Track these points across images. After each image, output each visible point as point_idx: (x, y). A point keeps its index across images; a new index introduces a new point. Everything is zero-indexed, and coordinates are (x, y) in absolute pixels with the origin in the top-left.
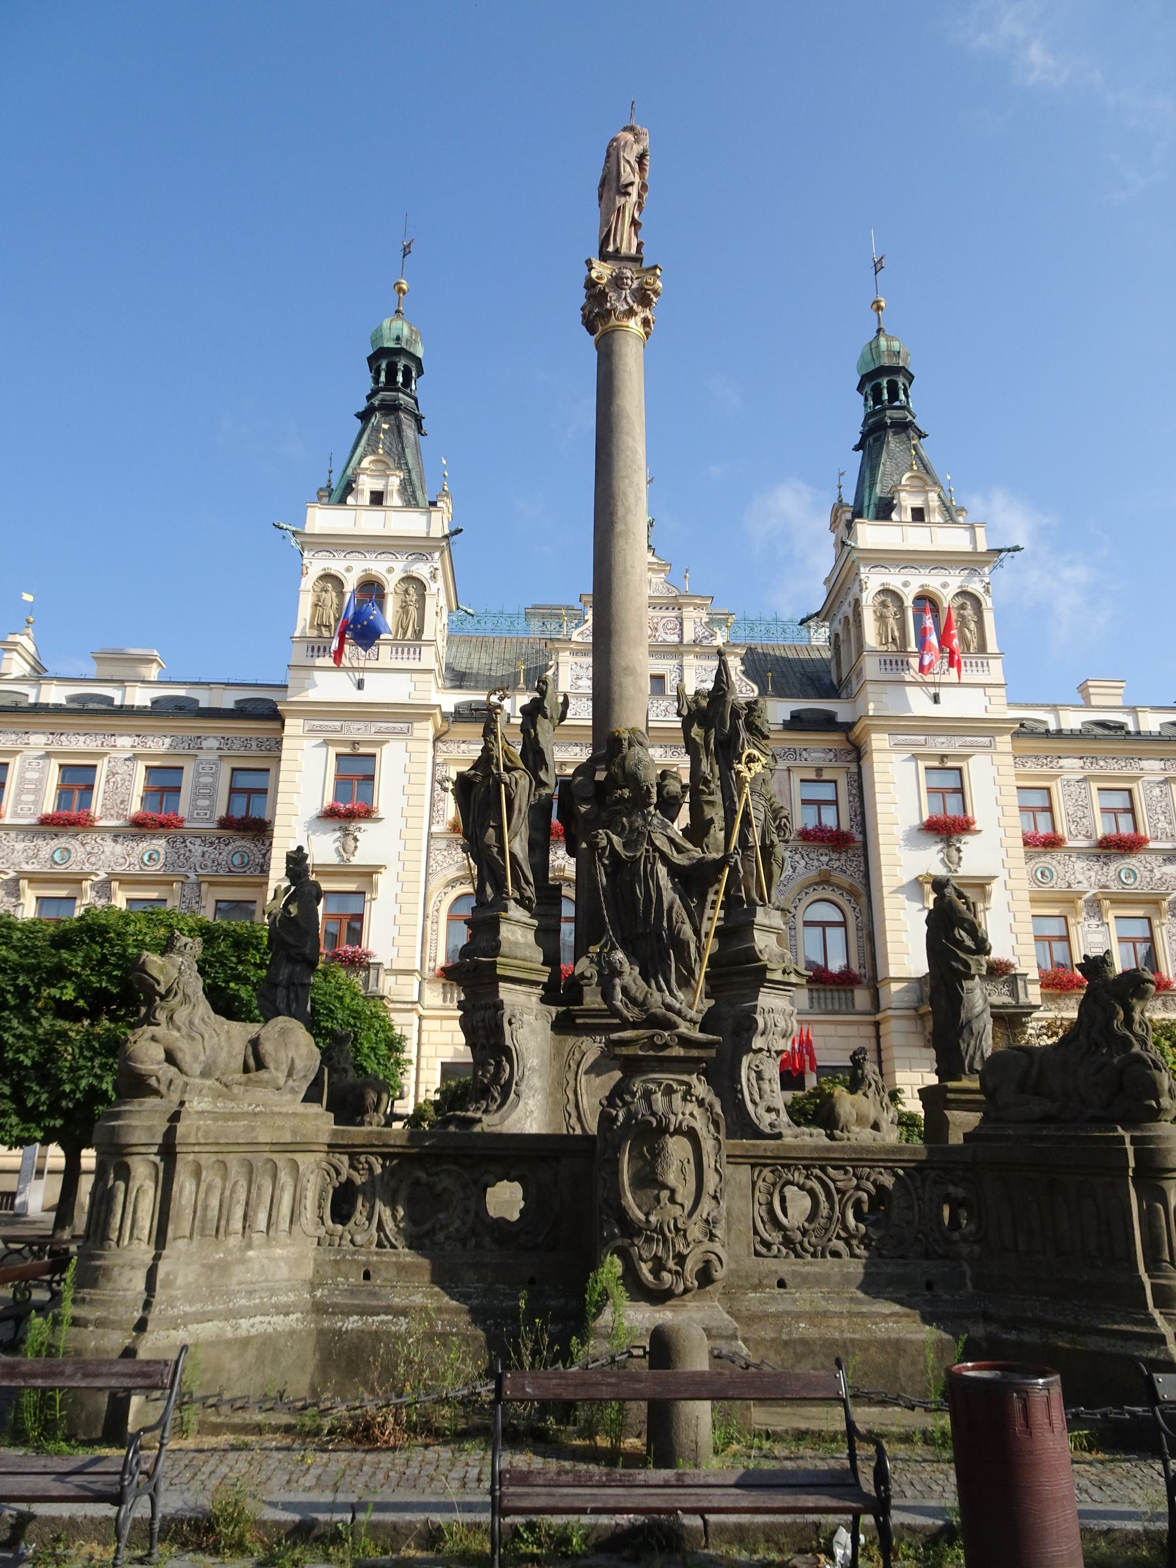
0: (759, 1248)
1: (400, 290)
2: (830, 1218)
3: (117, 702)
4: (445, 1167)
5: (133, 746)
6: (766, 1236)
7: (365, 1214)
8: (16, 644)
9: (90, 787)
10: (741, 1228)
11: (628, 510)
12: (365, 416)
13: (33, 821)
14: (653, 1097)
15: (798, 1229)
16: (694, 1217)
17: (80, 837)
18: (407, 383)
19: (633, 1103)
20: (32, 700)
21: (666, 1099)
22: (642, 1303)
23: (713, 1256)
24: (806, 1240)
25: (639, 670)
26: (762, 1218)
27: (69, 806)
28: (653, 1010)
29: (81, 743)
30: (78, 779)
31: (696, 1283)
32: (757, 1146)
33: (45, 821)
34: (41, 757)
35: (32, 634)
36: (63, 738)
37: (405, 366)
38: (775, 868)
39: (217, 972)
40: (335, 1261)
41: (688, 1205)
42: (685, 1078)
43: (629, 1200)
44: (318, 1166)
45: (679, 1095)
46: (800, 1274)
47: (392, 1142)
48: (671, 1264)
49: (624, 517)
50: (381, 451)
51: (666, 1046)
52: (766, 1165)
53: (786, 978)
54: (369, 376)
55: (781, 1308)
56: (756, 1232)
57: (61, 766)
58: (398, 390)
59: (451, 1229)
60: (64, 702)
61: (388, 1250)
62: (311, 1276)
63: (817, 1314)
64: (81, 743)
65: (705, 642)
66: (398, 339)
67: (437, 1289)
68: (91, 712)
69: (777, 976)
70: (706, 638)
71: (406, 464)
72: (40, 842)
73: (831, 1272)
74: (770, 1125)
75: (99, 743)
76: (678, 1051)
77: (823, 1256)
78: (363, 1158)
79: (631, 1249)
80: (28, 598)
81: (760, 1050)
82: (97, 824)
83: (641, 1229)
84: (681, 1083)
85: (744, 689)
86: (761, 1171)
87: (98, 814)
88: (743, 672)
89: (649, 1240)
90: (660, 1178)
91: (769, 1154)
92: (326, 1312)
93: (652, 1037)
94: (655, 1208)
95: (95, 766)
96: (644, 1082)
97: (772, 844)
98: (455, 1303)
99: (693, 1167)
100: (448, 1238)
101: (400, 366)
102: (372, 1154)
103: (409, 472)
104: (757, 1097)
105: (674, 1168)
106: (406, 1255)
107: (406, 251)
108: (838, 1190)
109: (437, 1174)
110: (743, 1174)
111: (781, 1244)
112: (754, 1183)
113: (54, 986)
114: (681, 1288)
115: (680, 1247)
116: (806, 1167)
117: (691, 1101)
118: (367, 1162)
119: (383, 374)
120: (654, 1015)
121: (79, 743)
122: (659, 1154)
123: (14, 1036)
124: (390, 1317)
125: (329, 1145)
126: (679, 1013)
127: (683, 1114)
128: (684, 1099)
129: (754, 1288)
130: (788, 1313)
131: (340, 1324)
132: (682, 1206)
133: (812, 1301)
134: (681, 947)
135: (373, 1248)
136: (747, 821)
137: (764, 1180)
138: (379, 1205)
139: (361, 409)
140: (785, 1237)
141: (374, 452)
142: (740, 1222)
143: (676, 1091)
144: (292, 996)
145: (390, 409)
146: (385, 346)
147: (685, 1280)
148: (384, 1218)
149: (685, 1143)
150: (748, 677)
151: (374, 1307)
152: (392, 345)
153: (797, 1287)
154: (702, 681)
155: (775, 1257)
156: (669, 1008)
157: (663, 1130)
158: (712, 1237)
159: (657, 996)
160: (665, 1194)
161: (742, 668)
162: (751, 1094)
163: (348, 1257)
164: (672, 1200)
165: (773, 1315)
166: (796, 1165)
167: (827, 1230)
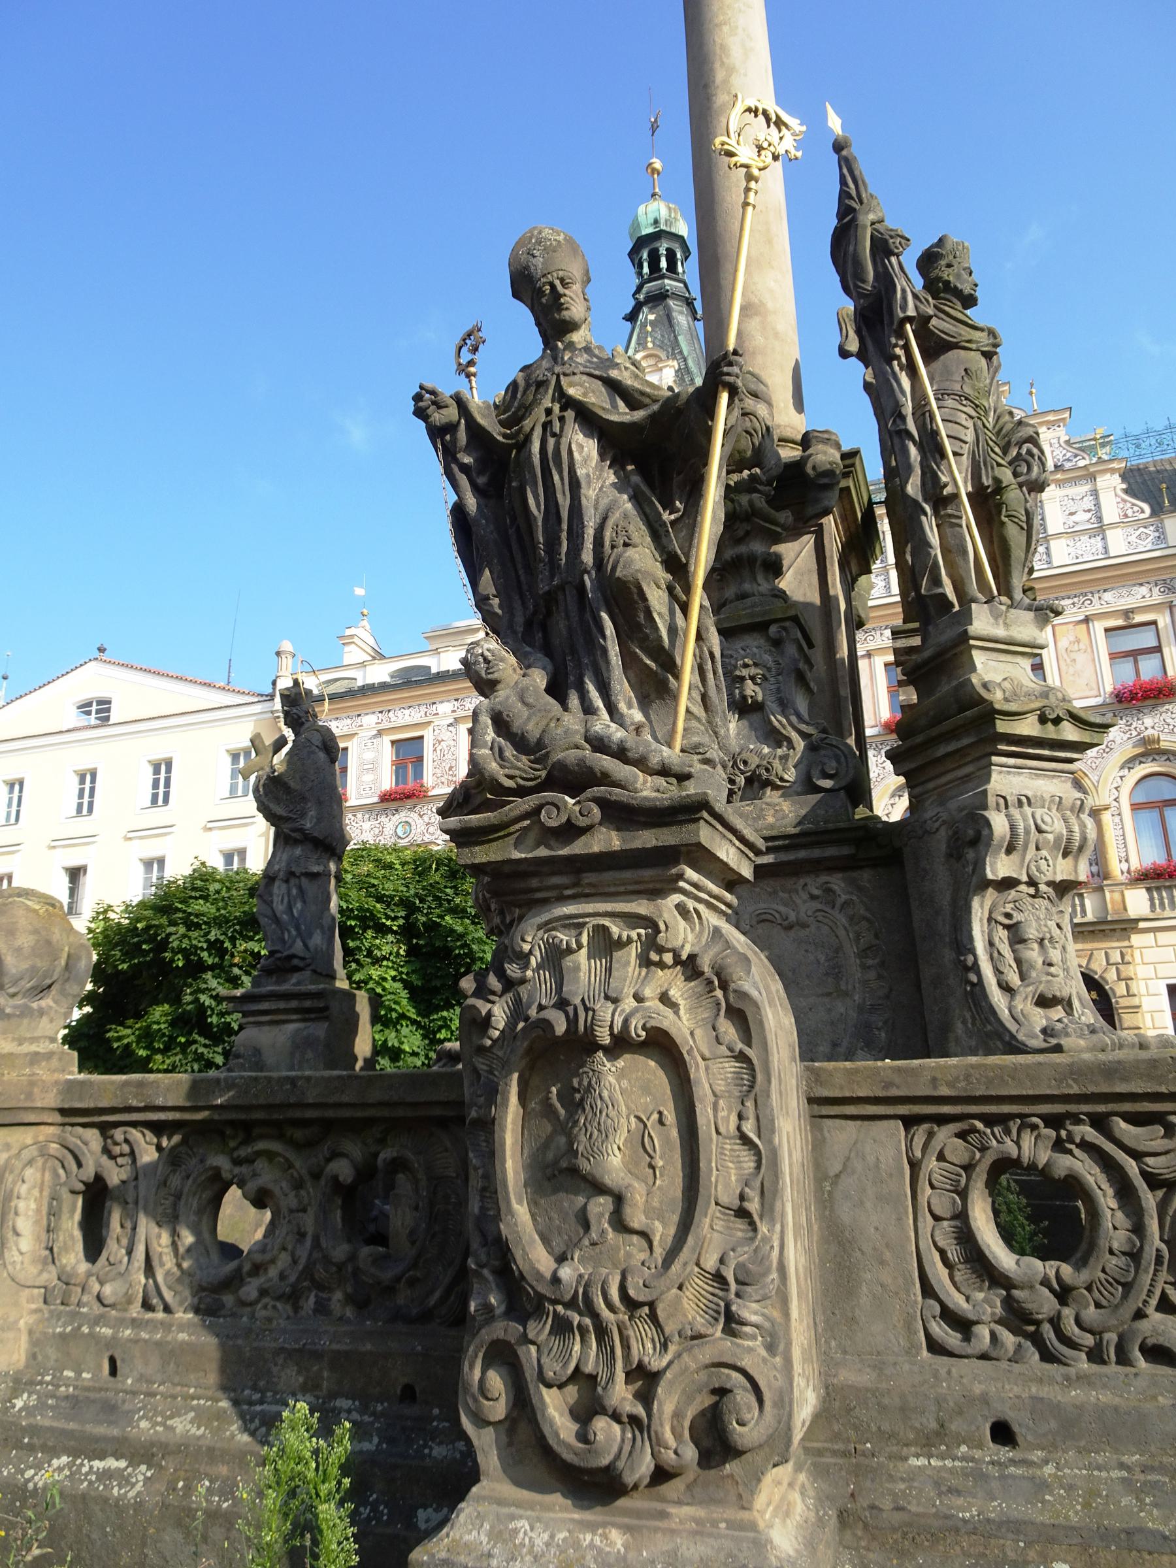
0: (939, 1330)
1: (654, 170)
2: (1135, 1256)
3: (434, 670)
4: (261, 1145)
5: (454, 711)
6: (957, 1301)
7: (125, 1242)
8: (352, 636)
9: (420, 759)
10: (886, 1276)
11: (731, 70)
12: (632, 317)
13: (376, 800)
14: (568, 962)
15: (1045, 1282)
16: (675, 1268)
17: (417, 809)
18: (672, 267)
19: (523, 981)
20: (360, 683)
21: (599, 965)
22: (557, 1498)
23: (735, 1375)
24: (1068, 1313)
25: (770, 305)
26: (942, 1252)
27: (405, 782)
28: (557, 756)
29: (407, 717)
30: (409, 753)
31: (690, 1453)
32: (912, 1072)
33: (386, 798)
34: (375, 737)
35: (368, 627)
36: (391, 714)
37: (667, 250)
38: (1014, 534)
39: (430, 908)
40: (63, 1336)
41: (663, 1233)
42: (641, 907)
43: (519, 1214)
44: (43, 1153)
45: (633, 951)
46: (1056, 1409)
47: (160, 1102)
48: (621, 1394)
49: (726, 81)
50: (650, 345)
51: (571, 831)
52: (942, 1120)
53: (1050, 732)
54: (631, 270)
55: (995, 1508)
56: (928, 1290)
57: (393, 742)
58: (663, 277)
59: (273, 1272)
60: (388, 680)
61: (160, 1315)
62: (22, 1364)
63: (1106, 1535)
64: (407, 717)
65: (1067, 465)
66: (656, 222)
67: (224, 1404)
68: (414, 681)
69: (1028, 727)
70: (1069, 460)
71: (681, 352)
72: (383, 819)
73: (1148, 1406)
74: (1044, 1031)
75: (423, 713)
76: (606, 840)
77: (1123, 1359)
78: (118, 1134)
79: (521, 1351)
80: (359, 592)
81: (1008, 884)
82: (430, 794)
83: (541, 1298)
84: (633, 920)
85: (1130, 513)
86: (931, 1135)
87: (430, 784)
88: (1126, 491)
89: (562, 1328)
90: (584, 1166)
91: (944, 1091)
92: (19, 1446)
93: (537, 810)
94: (578, 1244)
95: (422, 737)
96: (547, 926)
97: (999, 488)
98: (245, 1438)
99: (674, 1133)
100: (263, 1292)
101: (663, 251)
102: (134, 1124)
103: (685, 360)
104: (1014, 979)
105: (621, 1138)
106: (182, 1328)
107: (654, 128)
108: (1153, 1181)
109: (249, 1161)
110: (887, 1142)
111: (999, 1322)
112: (915, 1165)
113: (251, 939)
114: (646, 1466)
115: (645, 1350)
116: (1054, 1122)
117: (661, 965)
118: (126, 1141)
119: (646, 265)
120: (561, 766)
121: (405, 716)
122: (581, 1105)
123: (211, 997)
124: (122, 1464)
125: (63, 1112)
126: (621, 754)
127: (638, 998)
128: (645, 962)
129: (929, 1442)
130: (1016, 1527)
131: (29, 1473)
132: (645, 1235)
133: (1093, 1493)
134: (626, 600)
135: (136, 1310)
136: (932, 447)
137: (941, 1157)
138: (145, 1225)
139: (628, 310)
140: (1009, 1303)
141: (645, 348)
142: (882, 1263)
143: (620, 944)
144: (294, 891)
145: (658, 298)
146: (644, 233)
147: (657, 1443)
148: (156, 1249)
149: (650, 1069)
150: (1135, 496)
151: (97, 1439)
152: (650, 230)
153: (1051, 1447)
154: (1071, 514)
155: (984, 1357)
156: (599, 745)
157: (581, 1046)
158: (732, 1323)
159: (573, 721)
160: (600, 1206)
161: (1124, 486)
162: (998, 972)
163: (85, 1329)
164: (620, 1224)
165: (973, 1529)
166: (1022, 1116)
167: (1127, 1287)
